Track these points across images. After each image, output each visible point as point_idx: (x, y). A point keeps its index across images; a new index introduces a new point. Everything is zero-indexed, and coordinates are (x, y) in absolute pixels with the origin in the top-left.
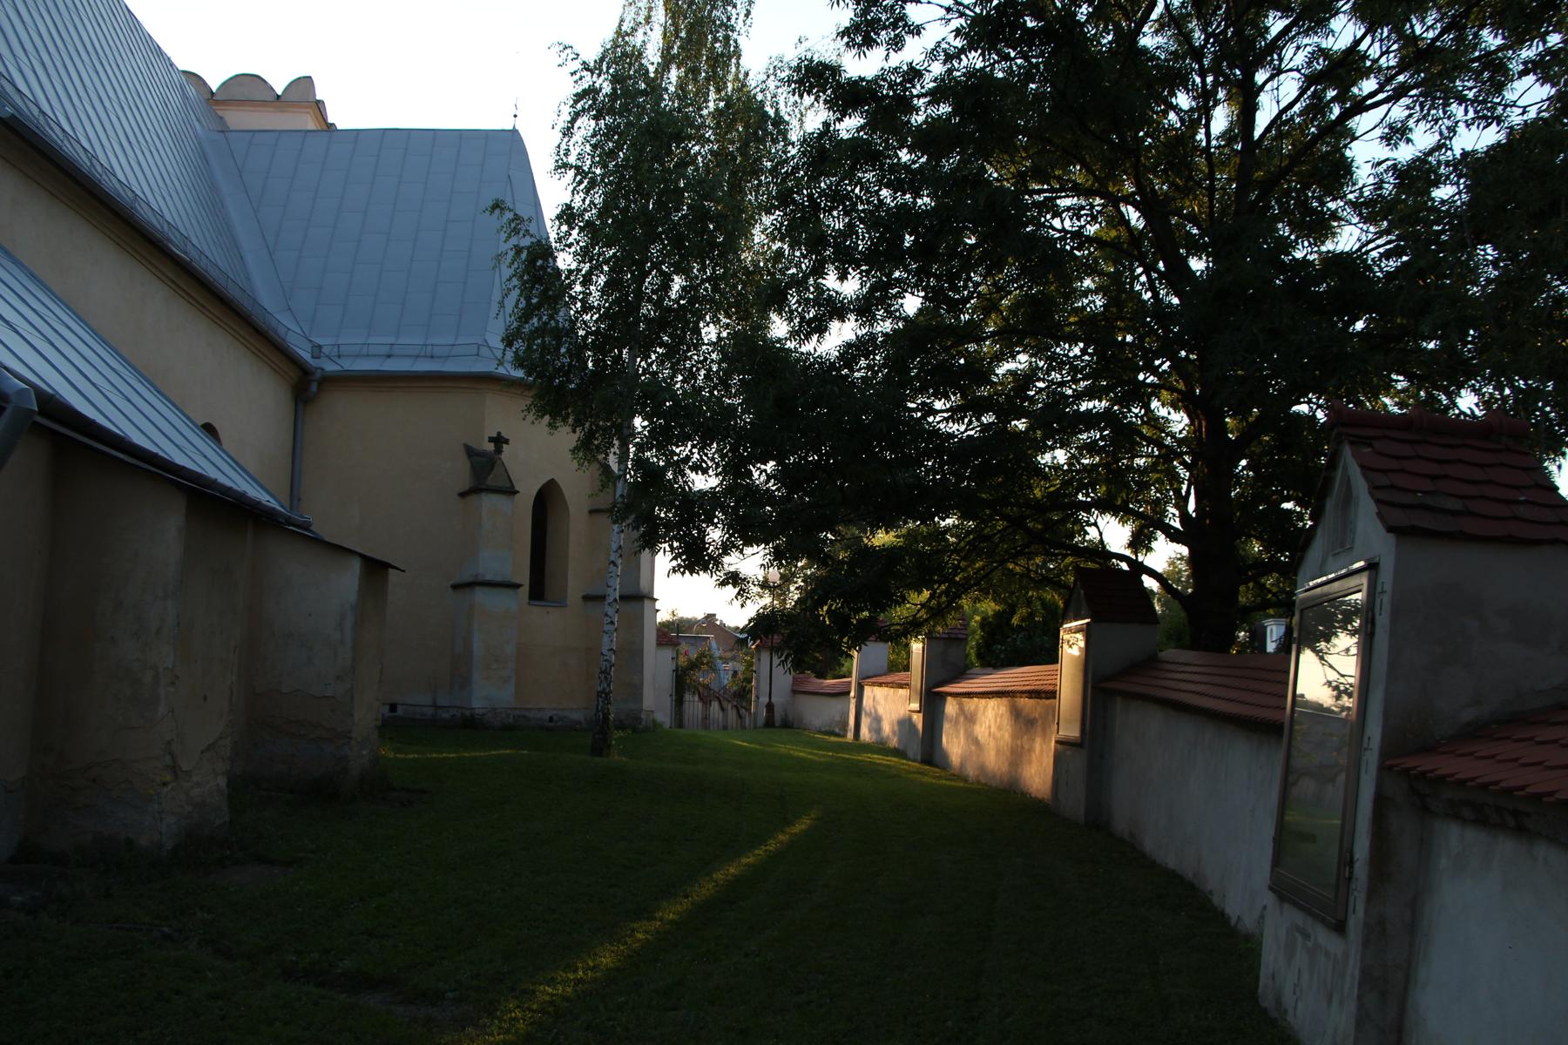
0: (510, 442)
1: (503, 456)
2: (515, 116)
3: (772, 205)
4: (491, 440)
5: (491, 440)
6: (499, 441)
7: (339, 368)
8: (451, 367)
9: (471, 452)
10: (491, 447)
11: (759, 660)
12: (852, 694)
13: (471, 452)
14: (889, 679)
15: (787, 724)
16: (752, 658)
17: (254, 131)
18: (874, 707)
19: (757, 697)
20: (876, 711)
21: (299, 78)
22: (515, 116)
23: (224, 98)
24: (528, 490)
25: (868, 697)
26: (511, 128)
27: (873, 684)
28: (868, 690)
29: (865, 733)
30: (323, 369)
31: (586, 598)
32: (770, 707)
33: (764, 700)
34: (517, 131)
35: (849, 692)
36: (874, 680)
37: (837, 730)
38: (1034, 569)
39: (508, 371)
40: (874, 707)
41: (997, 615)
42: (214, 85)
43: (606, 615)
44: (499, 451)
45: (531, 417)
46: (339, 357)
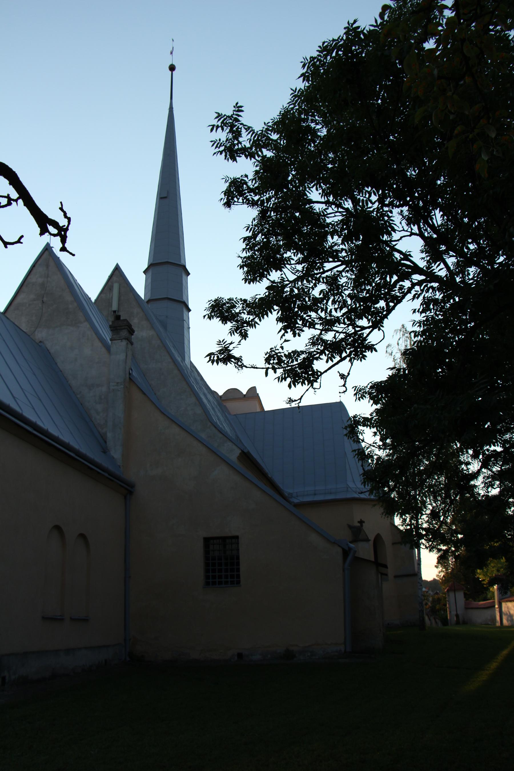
0: (365, 522)
1: (364, 527)
2: (340, 396)
3: (348, 307)
4: (359, 522)
5: (359, 522)
6: (361, 522)
7: (299, 501)
8: (338, 497)
9: (350, 527)
10: (359, 525)
11: (449, 596)
12: (497, 606)
13: (350, 527)
14: (510, 599)
15: (465, 623)
16: (445, 595)
17: (246, 414)
18: (508, 611)
19: (450, 612)
20: (510, 613)
21: (251, 388)
22: (340, 396)
23: (225, 399)
24: (372, 537)
25: (505, 607)
26: (339, 401)
27: (507, 601)
28: (504, 604)
29: (505, 622)
30: (293, 502)
31: (396, 577)
32: (457, 616)
33: (454, 613)
34: (342, 402)
35: (494, 606)
36: (506, 599)
37: (490, 623)
38: (429, 232)
39: (359, 496)
40: (508, 611)
41: (396, 492)
42: (221, 393)
43: (419, 583)
44: (362, 526)
45: (383, 516)
46: (297, 496)
